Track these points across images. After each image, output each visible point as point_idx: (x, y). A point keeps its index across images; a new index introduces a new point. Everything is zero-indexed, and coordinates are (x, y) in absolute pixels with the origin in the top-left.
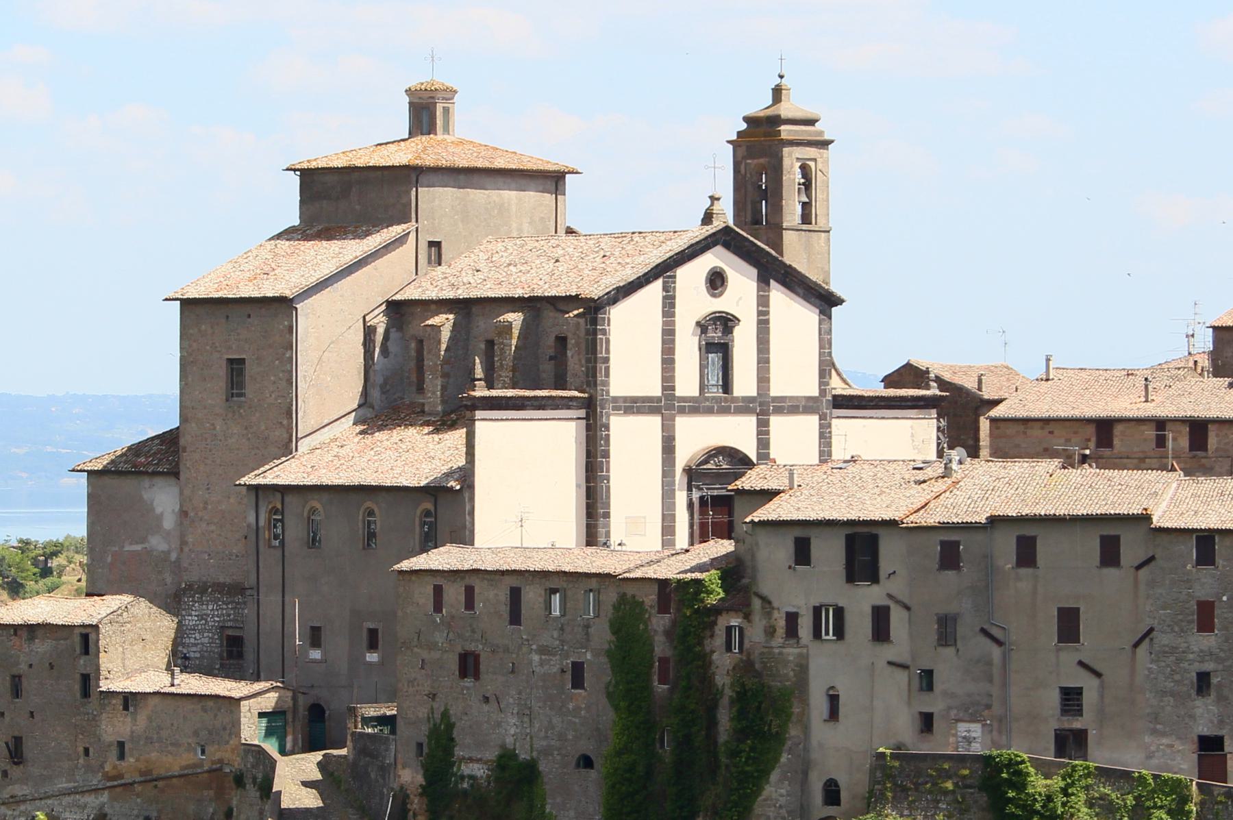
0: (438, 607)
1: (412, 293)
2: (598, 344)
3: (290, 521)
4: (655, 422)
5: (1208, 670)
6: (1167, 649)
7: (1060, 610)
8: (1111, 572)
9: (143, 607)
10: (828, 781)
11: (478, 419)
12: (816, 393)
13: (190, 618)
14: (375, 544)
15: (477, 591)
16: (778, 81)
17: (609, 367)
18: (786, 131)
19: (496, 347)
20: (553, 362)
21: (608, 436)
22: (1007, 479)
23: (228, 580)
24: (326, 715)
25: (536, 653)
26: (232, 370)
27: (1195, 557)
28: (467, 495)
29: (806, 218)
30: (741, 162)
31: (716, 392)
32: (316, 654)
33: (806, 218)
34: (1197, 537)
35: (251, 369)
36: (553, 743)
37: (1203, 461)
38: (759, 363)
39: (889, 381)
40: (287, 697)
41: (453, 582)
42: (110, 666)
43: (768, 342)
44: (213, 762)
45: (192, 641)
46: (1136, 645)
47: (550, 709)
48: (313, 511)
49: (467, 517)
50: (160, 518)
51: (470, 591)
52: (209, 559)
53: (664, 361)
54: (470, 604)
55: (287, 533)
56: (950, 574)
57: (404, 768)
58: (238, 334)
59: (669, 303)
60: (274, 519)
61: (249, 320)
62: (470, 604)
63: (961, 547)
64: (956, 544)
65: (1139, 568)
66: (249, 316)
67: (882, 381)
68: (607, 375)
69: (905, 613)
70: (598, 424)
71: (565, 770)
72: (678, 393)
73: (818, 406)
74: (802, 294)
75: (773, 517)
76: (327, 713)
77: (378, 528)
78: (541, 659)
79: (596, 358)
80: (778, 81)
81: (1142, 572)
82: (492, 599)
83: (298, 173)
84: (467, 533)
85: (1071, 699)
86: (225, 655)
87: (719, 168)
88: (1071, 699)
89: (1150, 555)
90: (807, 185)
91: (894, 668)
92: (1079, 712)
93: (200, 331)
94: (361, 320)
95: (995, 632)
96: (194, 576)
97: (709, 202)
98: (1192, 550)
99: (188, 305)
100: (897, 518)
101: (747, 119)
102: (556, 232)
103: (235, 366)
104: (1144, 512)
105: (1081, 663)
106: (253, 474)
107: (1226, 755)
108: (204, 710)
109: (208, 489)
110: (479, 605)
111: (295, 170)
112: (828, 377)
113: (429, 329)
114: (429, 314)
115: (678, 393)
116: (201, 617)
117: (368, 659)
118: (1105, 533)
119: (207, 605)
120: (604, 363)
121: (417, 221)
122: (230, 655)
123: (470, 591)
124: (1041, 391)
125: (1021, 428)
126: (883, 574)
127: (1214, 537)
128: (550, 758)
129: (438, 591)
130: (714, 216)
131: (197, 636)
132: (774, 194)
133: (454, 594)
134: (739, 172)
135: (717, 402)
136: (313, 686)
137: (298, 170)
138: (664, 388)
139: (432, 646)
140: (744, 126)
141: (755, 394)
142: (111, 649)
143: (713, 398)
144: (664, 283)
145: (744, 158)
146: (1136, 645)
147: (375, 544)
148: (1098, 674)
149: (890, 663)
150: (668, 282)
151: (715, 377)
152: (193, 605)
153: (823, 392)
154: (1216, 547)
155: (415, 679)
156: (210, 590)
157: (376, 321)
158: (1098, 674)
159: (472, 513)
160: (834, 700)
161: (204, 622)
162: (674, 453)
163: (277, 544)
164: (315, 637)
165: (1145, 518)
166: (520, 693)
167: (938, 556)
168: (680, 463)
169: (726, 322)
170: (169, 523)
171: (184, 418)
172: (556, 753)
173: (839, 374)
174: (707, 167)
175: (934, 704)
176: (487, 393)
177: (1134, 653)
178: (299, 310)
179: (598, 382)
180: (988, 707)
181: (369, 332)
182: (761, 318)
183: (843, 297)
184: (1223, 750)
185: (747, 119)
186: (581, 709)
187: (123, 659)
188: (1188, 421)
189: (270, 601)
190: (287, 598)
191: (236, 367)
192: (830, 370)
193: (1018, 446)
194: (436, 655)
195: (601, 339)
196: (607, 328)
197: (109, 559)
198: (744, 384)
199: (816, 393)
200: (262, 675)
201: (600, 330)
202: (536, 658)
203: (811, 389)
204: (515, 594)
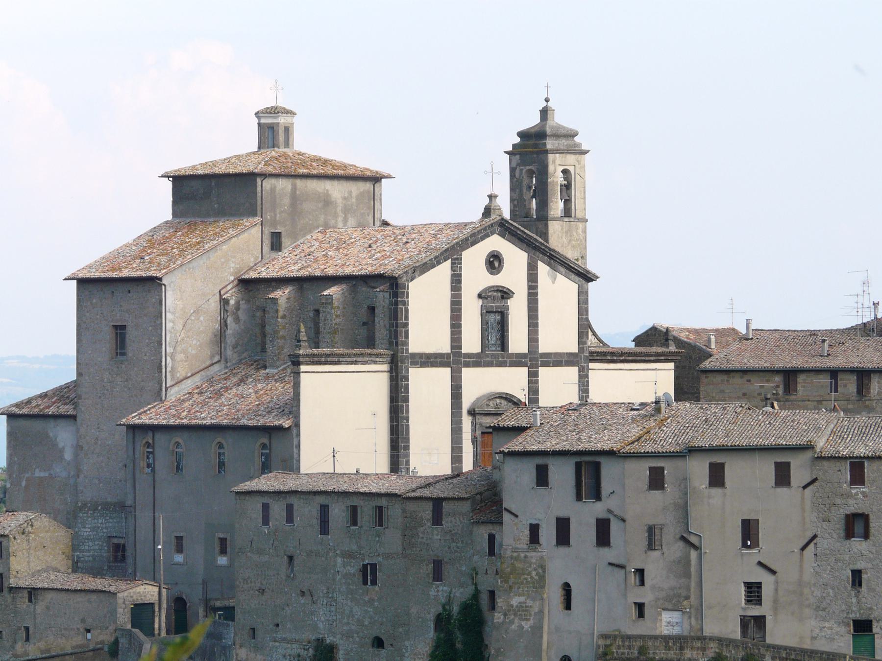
0: (266, 521)
1: (265, 273)
2: (399, 313)
3: (159, 452)
4: (445, 373)
5: (859, 568)
6: (828, 552)
7: (743, 520)
8: (782, 491)
9: (43, 522)
10: (563, 657)
11: (303, 372)
12: (575, 349)
13: (84, 530)
14: (224, 471)
15: (295, 508)
16: (545, 104)
17: (408, 331)
18: (550, 144)
19: (321, 315)
20: (366, 327)
21: (408, 385)
22: (705, 417)
23: (115, 500)
24: (187, 606)
25: (340, 557)
26: (117, 333)
27: (849, 479)
28: (295, 432)
29: (567, 212)
30: (516, 169)
31: (494, 350)
32: (179, 558)
33: (567, 212)
34: (850, 462)
35: (131, 334)
36: (353, 627)
37: (867, 403)
38: (529, 326)
39: (639, 340)
40: (154, 592)
41: (277, 501)
42: (19, 568)
43: (537, 310)
44: (97, 643)
45: (86, 548)
46: (803, 549)
47: (351, 601)
48: (178, 444)
49: (295, 450)
50: (62, 451)
51: (290, 508)
52: (99, 484)
53: (452, 326)
54: (290, 519)
55: (157, 463)
56: (657, 494)
57: (241, 647)
58: (121, 306)
59: (456, 281)
60: (147, 452)
61: (129, 295)
62: (290, 519)
63: (666, 472)
64: (662, 469)
65: (805, 487)
66: (129, 292)
67: (633, 341)
68: (407, 337)
69: (621, 524)
70: (399, 375)
71: (363, 649)
72: (464, 351)
73: (578, 361)
74: (563, 273)
75: (519, 448)
76: (188, 604)
77: (226, 459)
78: (344, 561)
79: (397, 324)
80: (545, 104)
81: (807, 490)
83: (171, 179)
84: (295, 462)
85: (753, 591)
86: (112, 559)
87: (488, 173)
89: (814, 477)
90: (567, 187)
91: (242, 497)
92: (759, 602)
93: (92, 304)
94: (218, 295)
95: (693, 539)
96: (88, 495)
97: (487, 201)
98: (846, 473)
99: (83, 283)
100: (615, 449)
101: (521, 134)
102: (374, 225)
103: (586, 323)
104: (809, 443)
105: (760, 564)
106: (130, 416)
107: (874, 635)
108: (89, 601)
109: (98, 428)
110: (297, 519)
111: (168, 177)
112: (585, 337)
113: (269, 301)
114: (271, 289)
115: (464, 351)
116: (93, 529)
117: (219, 562)
118: (779, 460)
119: (98, 519)
120: (404, 327)
121: (262, 217)
122: (116, 559)
123: (290, 508)
124: (743, 348)
125: (725, 377)
126: (604, 492)
127: (863, 463)
128: (351, 640)
129: (266, 507)
130: (492, 210)
131: (91, 544)
132: (542, 193)
133: (278, 510)
134: (515, 176)
135: (495, 358)
136: (177, 584)
137: (171, 177)
138: (452, 347)
139: (260, 552)
140: (517, 140)
141: (526, 351)
142: (19, 554)
143: (492, 355)
144: (452, 263)
145: (518, 165)
146: (803, 549)
147: (224, 471)
148: (773, 572)
149: (610, 564)
150: (455, 263)
151: (493, 338)
152: (87, 520)
153: (581, 349)
154: (866, 471)
155: (249, 578)
156: (100, 508)
157: (228, 295)
158: (773, 572)
159: (298, 446)
160: (567, 589)
161: (95, 533)
162: (462, 398)
163: (150, 472)
164: (179, 545)
165: (808, 447)
166: (328, 589)
167: (647, 479)
168: (466, 404)
169: (505, 294)
170: (68, 455)
171: (79, 374)
172: (355, 635)
173: (594, 334)
174: (486, 172)
175: (646, 596)
176: (309, 351)
177: (802, 555)
178: (167, 287)
179: (399, 343)
180: (687, 598)
181: (224, 302)
182: (531, 291)
183: (598, 274)
184: (872, 632)
185: (521, 134)
186: (373, 600)
187: (29, 562)
188: (828, 370)
189: (143, 518)
190: (157, 514)
191: (120, 331)
192: (587, 333)
193: (722, 391)
194: (265, 558)
195: (401, 309)
196: (406, 299)
197: (24, 483)
198: (518, 342)
199: (575, 349)
200: (138, 574)
201: (400, 301)
202: (339, 560)
203: (572, 347)
204: (324, 510)
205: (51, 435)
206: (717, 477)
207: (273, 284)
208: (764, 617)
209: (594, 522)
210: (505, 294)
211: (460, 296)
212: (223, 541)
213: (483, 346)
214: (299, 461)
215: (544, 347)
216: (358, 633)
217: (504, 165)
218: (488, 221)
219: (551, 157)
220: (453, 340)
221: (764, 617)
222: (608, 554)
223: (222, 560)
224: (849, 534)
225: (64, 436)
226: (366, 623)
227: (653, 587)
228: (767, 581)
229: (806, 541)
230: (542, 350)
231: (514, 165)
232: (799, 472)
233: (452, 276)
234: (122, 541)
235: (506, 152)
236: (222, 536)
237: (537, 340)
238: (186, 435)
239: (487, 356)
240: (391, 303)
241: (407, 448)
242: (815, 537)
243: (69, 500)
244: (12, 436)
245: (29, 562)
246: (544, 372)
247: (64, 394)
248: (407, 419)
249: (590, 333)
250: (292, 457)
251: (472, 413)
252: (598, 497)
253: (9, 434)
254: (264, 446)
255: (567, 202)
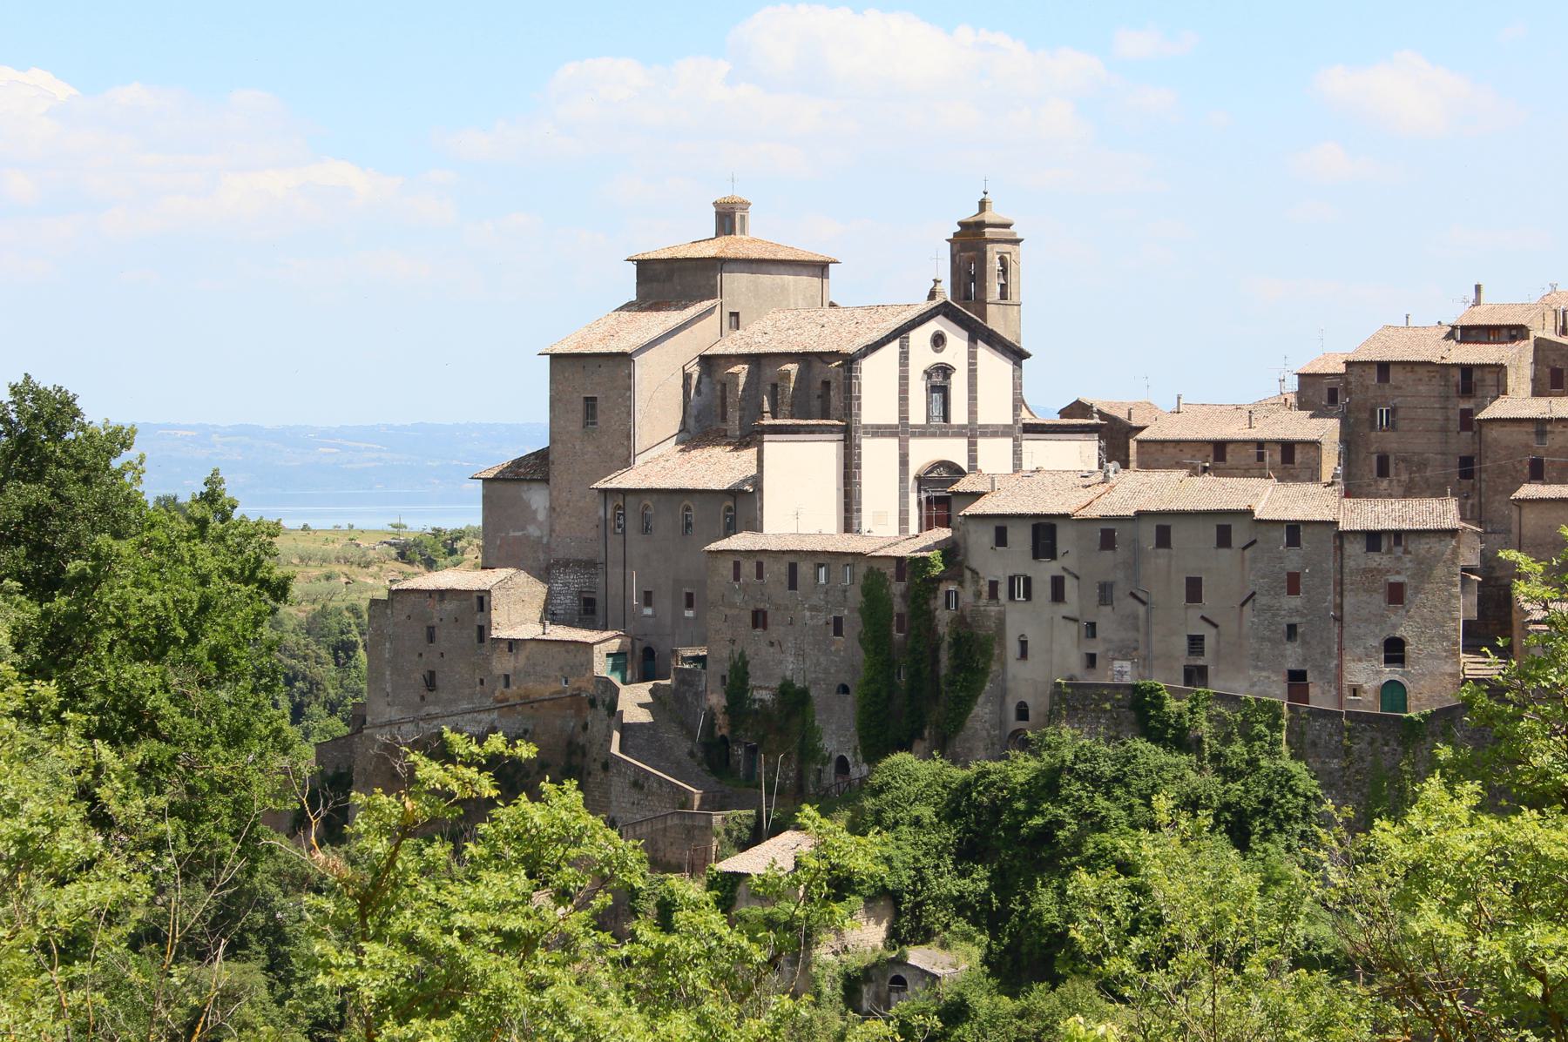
0: (737, 577)
3: (629, 514)
4: (894, 443)
8: (1224, 551)
9: (523, 577)
12: (1011, 422)
15: (765, 565)
29: (1004, 295)
31: (938, 421)
35: (601, 405)
39: (1064, 413)
44: (574, 690)
46: (1243, 604)
50: (535, 512)
51: (760, 566)
54: (760, 575)
55: (627, 524)
56: (1109, 553)
62: (760, 575)
65: (1245, 548)
68: (860, 409)
69: (1075, 581)
75: (980, 511)
76: (656, 654)
82: (778, 570)
85: (1196, 643)
88: (1196, 643)
90: (1004, 271)
92: (1202, 653)
95: (1140, 595)
101: (960, 224)
110: (767, 576)
111: (633, 261)
116: (565, 585)
118: (1220, 523)
122: (586, 612)
123: (760, 566)
125: (1160, 447)
126: (1059, 553)
129: (737, 565)
132: (980, 278)
133: (748, 568)
138: (900, 419)
141: (966, 423)
142: (499, 607)
143: (936, 426)
145: (959, 252)
146: (1243, 604)
148: (1216, 626)
149: (1064, 617)
151: (937, 410)
153: (1016, 421)
158: (1216, 626)
160: (1024, 644)
164: (648, 598)
169: (946, 370)
170: (541, 516)
173: (1027, 408)
175: (1097, 647)
177: (1241, 611)
180: (1136, 649)
181: (687, 377)
183: (1030, 352)
187: (509, 615)
189: (615, 573)
191: (590, 403)
198: (959, 416)
199: (1011, 422)
205: (525, 497)
206: (1163, 538)
207: (733, 359)
208: (1206, 667)
209: (1050, 579)
210: (946, 370)
211: (907, 371)
212: (690, 597)
213: (928, 418)
214: (762, 522)
215: (982, 420)
216: (824, 680)
217: (946, 249)
218: (934, 303)
219: (989, 246)
220: (901, 412)
221: (1206, 667)
222: (1064, 609)
223: (689, 613)
224: (755, 625)
225: (538, 499)
226: (832, 671)
227: (1105, 640)
228: (1209, 634)
229: (1245, 598)
230: (980, 422)
231: (955, 251)
232: (1239, 536)
233: (901, 353)
234: (591, 596)
235: (948, 240)
236: (689, 590)
237: (976, 413)
238: (655, 497)
239: (932, 426)
240: (845, 378)
241: (859, 510)
242: (1254, 593)
243: (542, 557)
244: (487, 499)
245: (509, 615)
246: (982, 443)
247: (542, 456)
248: (860, 484)
249: (1023, 407)
250: (756, 519)
251: (922, 481)
252: (1053, 556)
253: (485, 497)
254: (729, 509)
255: (1004, 287)
